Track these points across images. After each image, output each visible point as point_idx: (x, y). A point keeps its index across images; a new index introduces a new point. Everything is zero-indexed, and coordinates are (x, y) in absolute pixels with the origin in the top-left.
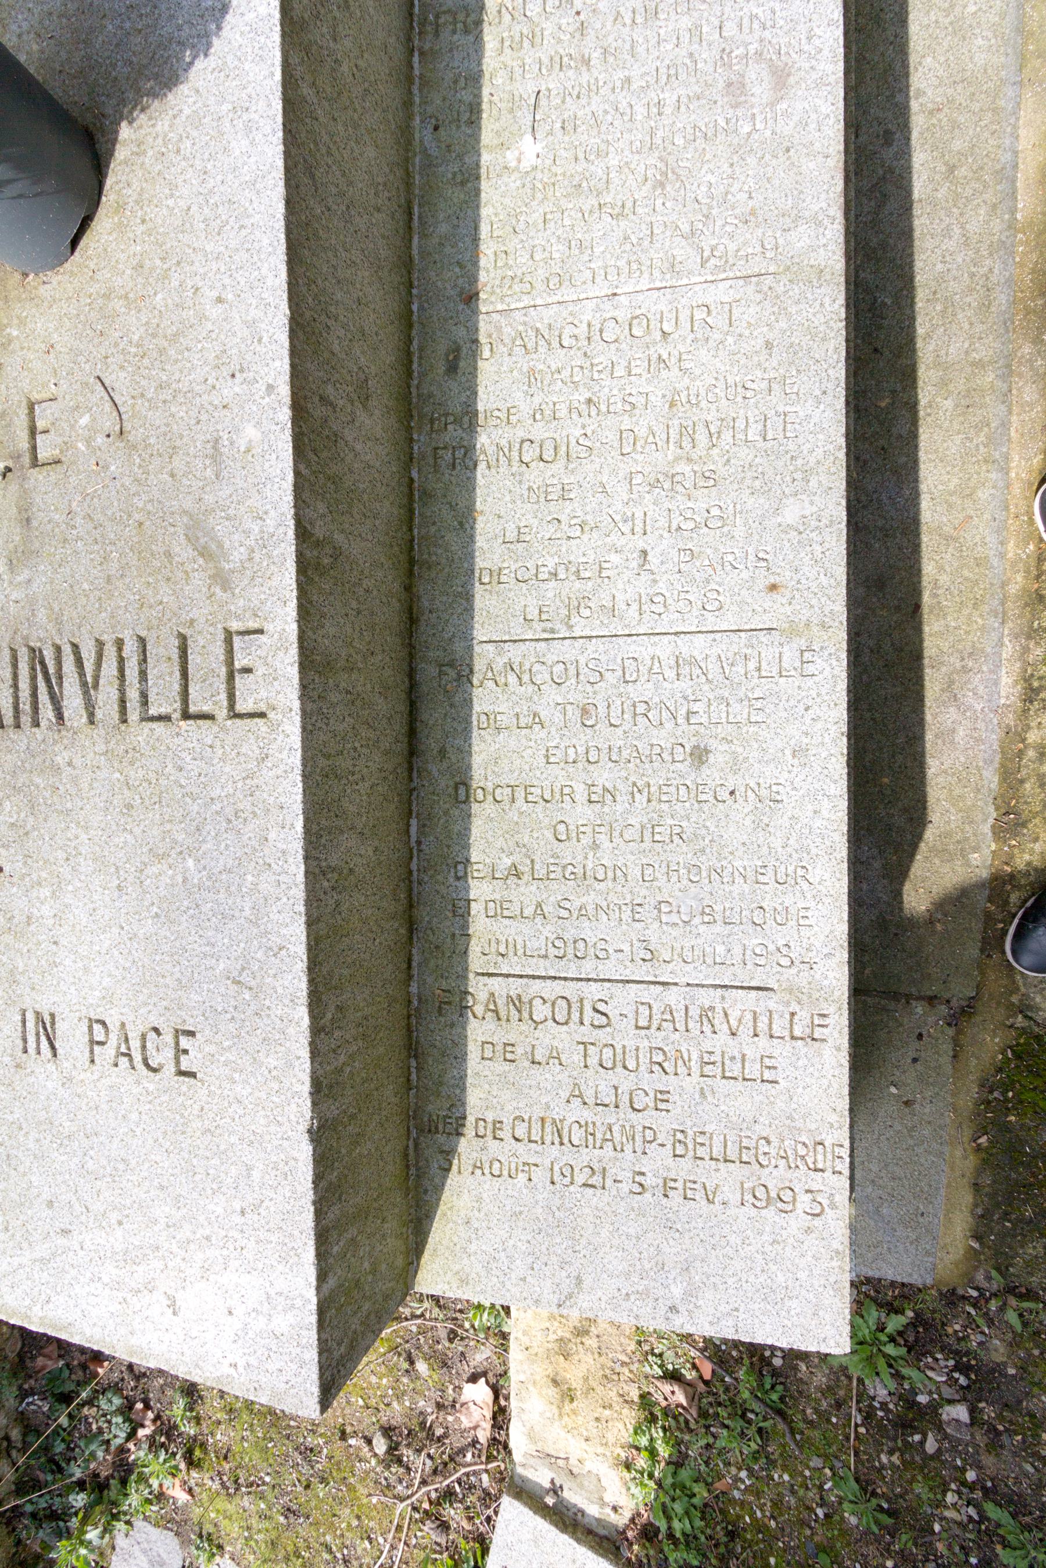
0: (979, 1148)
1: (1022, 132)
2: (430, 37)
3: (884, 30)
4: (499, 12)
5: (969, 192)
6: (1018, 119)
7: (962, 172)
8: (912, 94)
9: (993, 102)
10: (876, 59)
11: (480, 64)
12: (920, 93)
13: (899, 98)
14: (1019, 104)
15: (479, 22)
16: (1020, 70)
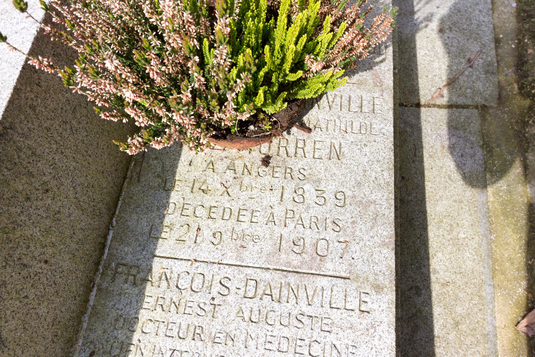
0: (521, 160)
1: (498, 316)
2: (109, 279)
3: (414, 229)
4: (160, 278)
5: (468, 342)
6: (494, 307)
7: (463, 327)
8: (431, 270)
9: (479, 292)
10: (410, 243)
11: (137, 313)
12: (436, 272)
13: (423, 270)
14: (494, 298)
15: (145, 280)
16: (493, 278)
